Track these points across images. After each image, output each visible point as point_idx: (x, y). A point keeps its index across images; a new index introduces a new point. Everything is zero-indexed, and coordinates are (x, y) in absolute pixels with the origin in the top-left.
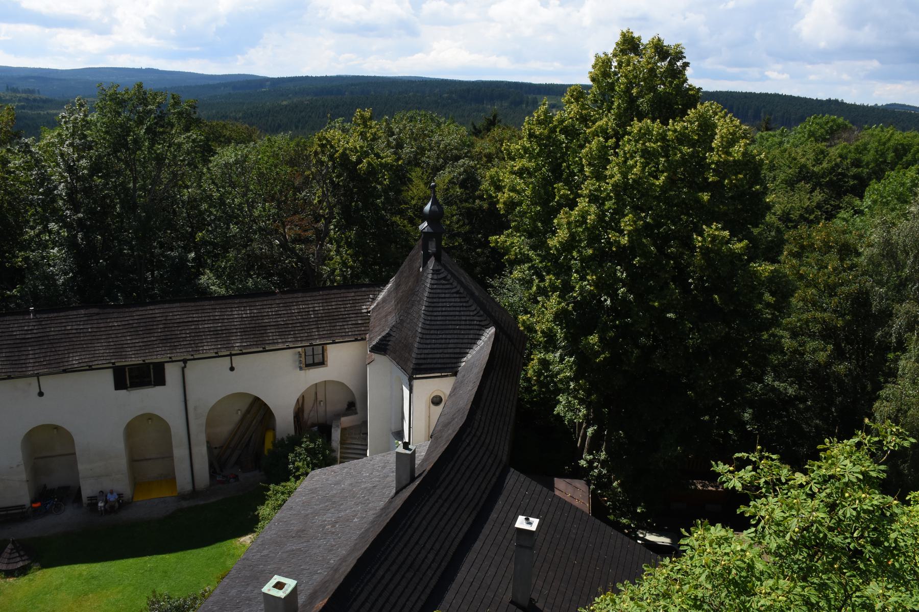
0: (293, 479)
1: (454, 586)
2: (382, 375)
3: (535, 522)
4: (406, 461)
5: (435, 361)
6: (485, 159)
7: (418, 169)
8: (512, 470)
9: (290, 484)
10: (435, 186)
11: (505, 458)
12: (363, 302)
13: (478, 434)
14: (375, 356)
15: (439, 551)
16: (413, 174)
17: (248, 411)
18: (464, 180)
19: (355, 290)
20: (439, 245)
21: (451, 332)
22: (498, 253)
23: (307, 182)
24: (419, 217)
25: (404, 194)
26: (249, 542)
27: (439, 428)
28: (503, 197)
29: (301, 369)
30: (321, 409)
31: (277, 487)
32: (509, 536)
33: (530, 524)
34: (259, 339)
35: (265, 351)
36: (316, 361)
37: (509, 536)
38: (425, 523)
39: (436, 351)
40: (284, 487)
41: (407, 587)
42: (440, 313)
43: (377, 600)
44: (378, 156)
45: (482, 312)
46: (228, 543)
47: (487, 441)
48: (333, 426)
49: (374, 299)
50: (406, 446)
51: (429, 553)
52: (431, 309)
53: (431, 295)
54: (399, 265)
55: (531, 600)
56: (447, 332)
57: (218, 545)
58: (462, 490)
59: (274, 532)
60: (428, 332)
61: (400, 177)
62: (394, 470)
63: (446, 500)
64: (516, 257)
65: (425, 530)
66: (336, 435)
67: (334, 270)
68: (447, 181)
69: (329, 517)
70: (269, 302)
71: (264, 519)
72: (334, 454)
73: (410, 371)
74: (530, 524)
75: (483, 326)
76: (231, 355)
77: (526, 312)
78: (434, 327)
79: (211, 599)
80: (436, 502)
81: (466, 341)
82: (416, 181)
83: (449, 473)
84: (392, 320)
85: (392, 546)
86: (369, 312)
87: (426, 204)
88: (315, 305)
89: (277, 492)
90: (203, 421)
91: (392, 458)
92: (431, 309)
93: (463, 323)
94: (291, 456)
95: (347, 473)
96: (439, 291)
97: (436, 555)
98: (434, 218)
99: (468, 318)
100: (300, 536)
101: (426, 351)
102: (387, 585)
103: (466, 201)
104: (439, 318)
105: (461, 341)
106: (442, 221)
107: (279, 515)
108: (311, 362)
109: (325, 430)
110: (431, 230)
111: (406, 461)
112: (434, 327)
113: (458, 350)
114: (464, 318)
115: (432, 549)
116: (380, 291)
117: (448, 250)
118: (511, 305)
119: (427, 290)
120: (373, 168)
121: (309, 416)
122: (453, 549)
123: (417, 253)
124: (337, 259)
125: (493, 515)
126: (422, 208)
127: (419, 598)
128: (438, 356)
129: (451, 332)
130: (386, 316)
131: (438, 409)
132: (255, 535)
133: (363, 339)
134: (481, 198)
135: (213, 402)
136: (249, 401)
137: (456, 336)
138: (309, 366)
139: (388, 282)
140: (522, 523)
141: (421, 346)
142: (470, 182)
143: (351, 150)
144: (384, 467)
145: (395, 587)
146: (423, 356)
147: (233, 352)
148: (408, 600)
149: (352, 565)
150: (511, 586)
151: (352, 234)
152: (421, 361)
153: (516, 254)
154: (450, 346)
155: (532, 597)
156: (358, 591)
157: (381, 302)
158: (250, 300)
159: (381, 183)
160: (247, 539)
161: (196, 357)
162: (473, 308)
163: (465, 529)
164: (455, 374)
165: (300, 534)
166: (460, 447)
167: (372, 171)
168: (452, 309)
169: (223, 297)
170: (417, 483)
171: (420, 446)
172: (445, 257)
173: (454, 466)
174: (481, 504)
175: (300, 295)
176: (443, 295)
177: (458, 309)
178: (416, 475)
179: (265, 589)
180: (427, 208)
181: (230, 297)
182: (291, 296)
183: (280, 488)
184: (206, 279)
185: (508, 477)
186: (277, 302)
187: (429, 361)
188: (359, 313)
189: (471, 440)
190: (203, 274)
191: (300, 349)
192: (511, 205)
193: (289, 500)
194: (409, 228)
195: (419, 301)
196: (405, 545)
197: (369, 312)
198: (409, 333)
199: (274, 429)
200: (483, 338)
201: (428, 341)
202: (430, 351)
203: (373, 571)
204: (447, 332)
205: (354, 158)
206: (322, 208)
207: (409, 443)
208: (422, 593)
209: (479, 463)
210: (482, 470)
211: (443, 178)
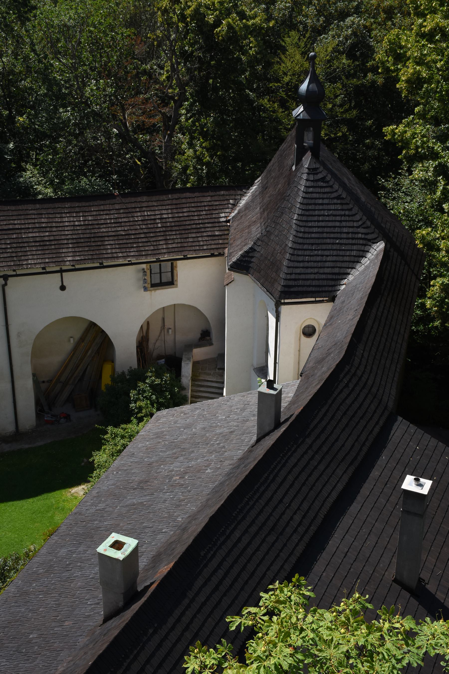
0: (135, 421)
1: (324, 557)
2: (243, 298)
3: (427, 484)
4: (270, 403)
5: (308, 283)
6: (383, 15)
7: (293, 33)
8: (400, 419)
9: (131, 427)
10: (314, 57)
11: (391, 404)
12: (222, 207)
13: (359, 373)
14: (235, 275)
15: (307, 512)
16: (287, 39)
17: (82, 339)
18: (353, 46)
19: (211, 193)
20: (317, 138)
21: (330, 247)
22: (393, 147)
23: (152, 53)
24: (294, 99)
25: (276, 67)
26: (82, 493)
27: (311, 364)
28: (406, 72)
29: (145, 289)
30: (169, 338)
31: (115, 430)
32: (393, 499)
33: (421, 485)
34: (95, 253)
35: (102, 267)
36: (164, 280)
37: (393, 499)
38: (291, 478)
39: (309, 271)
40: (124, 429)
41: (267, 553)
42: (316, 224)
43: (231, 567)
44: (242, 15)
45: (368, 223)
46: (57, 494)
47: (370, 382)
48: (184, 358)
49: (234, 205)
50: (270, 384)
51: (295, 513)
52: (304, 218)
53: (306, 201)
54: (267, 162)
55: (420, 580)
56: (324, 247)
57: (45, 496)
58: (337, 440)
59: (111, 482)
60: (300, 247)
61: (271, 44)
62: (256, 413)
63: (316, 452)
64: (417, 152)
65: (291, 486)
66: (187, 369)
67: (185, 168)
68: (330, 49)
69: (177, 466)
70: (107, 207)
71: (100, 467)
72: (183, 393)
73: (277, 295)
74: (421, 485)
75: (369, 240)
76: (61, 271)
77: (429, 223)
78: (308, 241)
79: (36, 559)
80: (306, 453)
81: (347, 259)
82: (291, 50)
83: (322, 419)
84: (256, 231)
85: (251, 503)
86: (228, 221)
87: (302, 82)
88: (162, 211)
89: (116, 435)
90: (29, 349)
91: (253, 399)
92: (304, 218)
93: (344, 236)
94: (133, 394)
95: (199, 415)
96: (314, 195)
97: (304, 517)
98: (312, 101)
99: (351, 230)
100: (142, 488)
101: (298, 271)
102: (245, 549)
103: (354, 76)
104: (315, 230)
105: (341, 259)
106: (321, 104)
107: (118, 462)
108: (158, 281)
109: (173, 363)
110: (307, 117)
111: (270, 403)
112: (308, 241)
113: (336, 270)
114: (345, 230)
115: (298, 509)
116: (242, 195)
117: (331, 143)
118: (407, 213)
119: (301, 194)
120: (235, 32)
121: (155, 346)
122: (324, 511)
123: (290, 146)
124: (191, 152)
125: (375, 473)
126: (297, 87)
127: (282, 567)
128: (312, 276)
129: (330, 247)
130: (249, 226)
131: (312, 341)
132: (89, 485)
133: (220, 255)
134: (374, 70)
135: (40, 327)
136: (84, 326)
137: (335, 253)
138: (154, 286)
139: (252, 184)
140: (410, 484)
141: (292, 264)
142: (359, 49)
143: (207, 7)
144: (243, 410)
145: (254, 554)
146: (293, 277)
147: (64, 268)
148: (268, 569)
149: (203, 524)
150: (395, 560)
151: (209, 121)
152: (291, 283)
153: (417, 147)
154: (327, 264)
155: (421, 576)
156: (210, 555)
157: (244, 208)
158: (84, 204)
159: (245, 53)
160: (79, 491)
161: (19, 272)
162: (358, 217)
163: (340, 487)
164: (332, 299)
165: (142, 485)
166: (336, 388)
167: (233, 37)
168: (331, 218)
169: (47, 200)
170: (283, 429)
171: (287, 386)
172: (324, 151)
173: (327, 411)
174: (360, 458)
175: (145, 198)
176: (320, 201)
177: (338, 218)
178: (282, 420)
179: (101, 549)
180: (304, 87)
181: (59, 200)
182: (133, 199)
183: (119, 431)
184: (30, 174)
185: (395, 427)
186: (117, 207)
187: (301, 283)
188: (216, 223)
189: (350, 381)
190: (25, 170)
191: (144, 266)
192: (416, 82)
193: (130, 445)
194: (280, 113)
195: (290, 209)
196: (267, 504)
197: (228, 221)
198: (278, 248)
199: (113, 361)
200: (369, 255)
201: (301, 259)
202: (303, 271)
203: (228, 531)
204: (324, 247)
205: (211, 19)
206: (171, 87)
207: (273, 382)
208: (286, 561)
209: (359, 408)
210: (362, 418)
211: (326, 45)
